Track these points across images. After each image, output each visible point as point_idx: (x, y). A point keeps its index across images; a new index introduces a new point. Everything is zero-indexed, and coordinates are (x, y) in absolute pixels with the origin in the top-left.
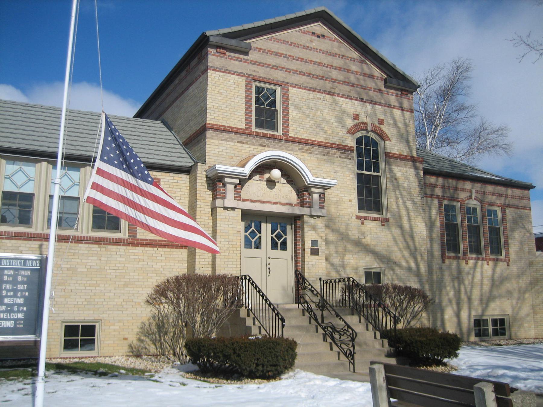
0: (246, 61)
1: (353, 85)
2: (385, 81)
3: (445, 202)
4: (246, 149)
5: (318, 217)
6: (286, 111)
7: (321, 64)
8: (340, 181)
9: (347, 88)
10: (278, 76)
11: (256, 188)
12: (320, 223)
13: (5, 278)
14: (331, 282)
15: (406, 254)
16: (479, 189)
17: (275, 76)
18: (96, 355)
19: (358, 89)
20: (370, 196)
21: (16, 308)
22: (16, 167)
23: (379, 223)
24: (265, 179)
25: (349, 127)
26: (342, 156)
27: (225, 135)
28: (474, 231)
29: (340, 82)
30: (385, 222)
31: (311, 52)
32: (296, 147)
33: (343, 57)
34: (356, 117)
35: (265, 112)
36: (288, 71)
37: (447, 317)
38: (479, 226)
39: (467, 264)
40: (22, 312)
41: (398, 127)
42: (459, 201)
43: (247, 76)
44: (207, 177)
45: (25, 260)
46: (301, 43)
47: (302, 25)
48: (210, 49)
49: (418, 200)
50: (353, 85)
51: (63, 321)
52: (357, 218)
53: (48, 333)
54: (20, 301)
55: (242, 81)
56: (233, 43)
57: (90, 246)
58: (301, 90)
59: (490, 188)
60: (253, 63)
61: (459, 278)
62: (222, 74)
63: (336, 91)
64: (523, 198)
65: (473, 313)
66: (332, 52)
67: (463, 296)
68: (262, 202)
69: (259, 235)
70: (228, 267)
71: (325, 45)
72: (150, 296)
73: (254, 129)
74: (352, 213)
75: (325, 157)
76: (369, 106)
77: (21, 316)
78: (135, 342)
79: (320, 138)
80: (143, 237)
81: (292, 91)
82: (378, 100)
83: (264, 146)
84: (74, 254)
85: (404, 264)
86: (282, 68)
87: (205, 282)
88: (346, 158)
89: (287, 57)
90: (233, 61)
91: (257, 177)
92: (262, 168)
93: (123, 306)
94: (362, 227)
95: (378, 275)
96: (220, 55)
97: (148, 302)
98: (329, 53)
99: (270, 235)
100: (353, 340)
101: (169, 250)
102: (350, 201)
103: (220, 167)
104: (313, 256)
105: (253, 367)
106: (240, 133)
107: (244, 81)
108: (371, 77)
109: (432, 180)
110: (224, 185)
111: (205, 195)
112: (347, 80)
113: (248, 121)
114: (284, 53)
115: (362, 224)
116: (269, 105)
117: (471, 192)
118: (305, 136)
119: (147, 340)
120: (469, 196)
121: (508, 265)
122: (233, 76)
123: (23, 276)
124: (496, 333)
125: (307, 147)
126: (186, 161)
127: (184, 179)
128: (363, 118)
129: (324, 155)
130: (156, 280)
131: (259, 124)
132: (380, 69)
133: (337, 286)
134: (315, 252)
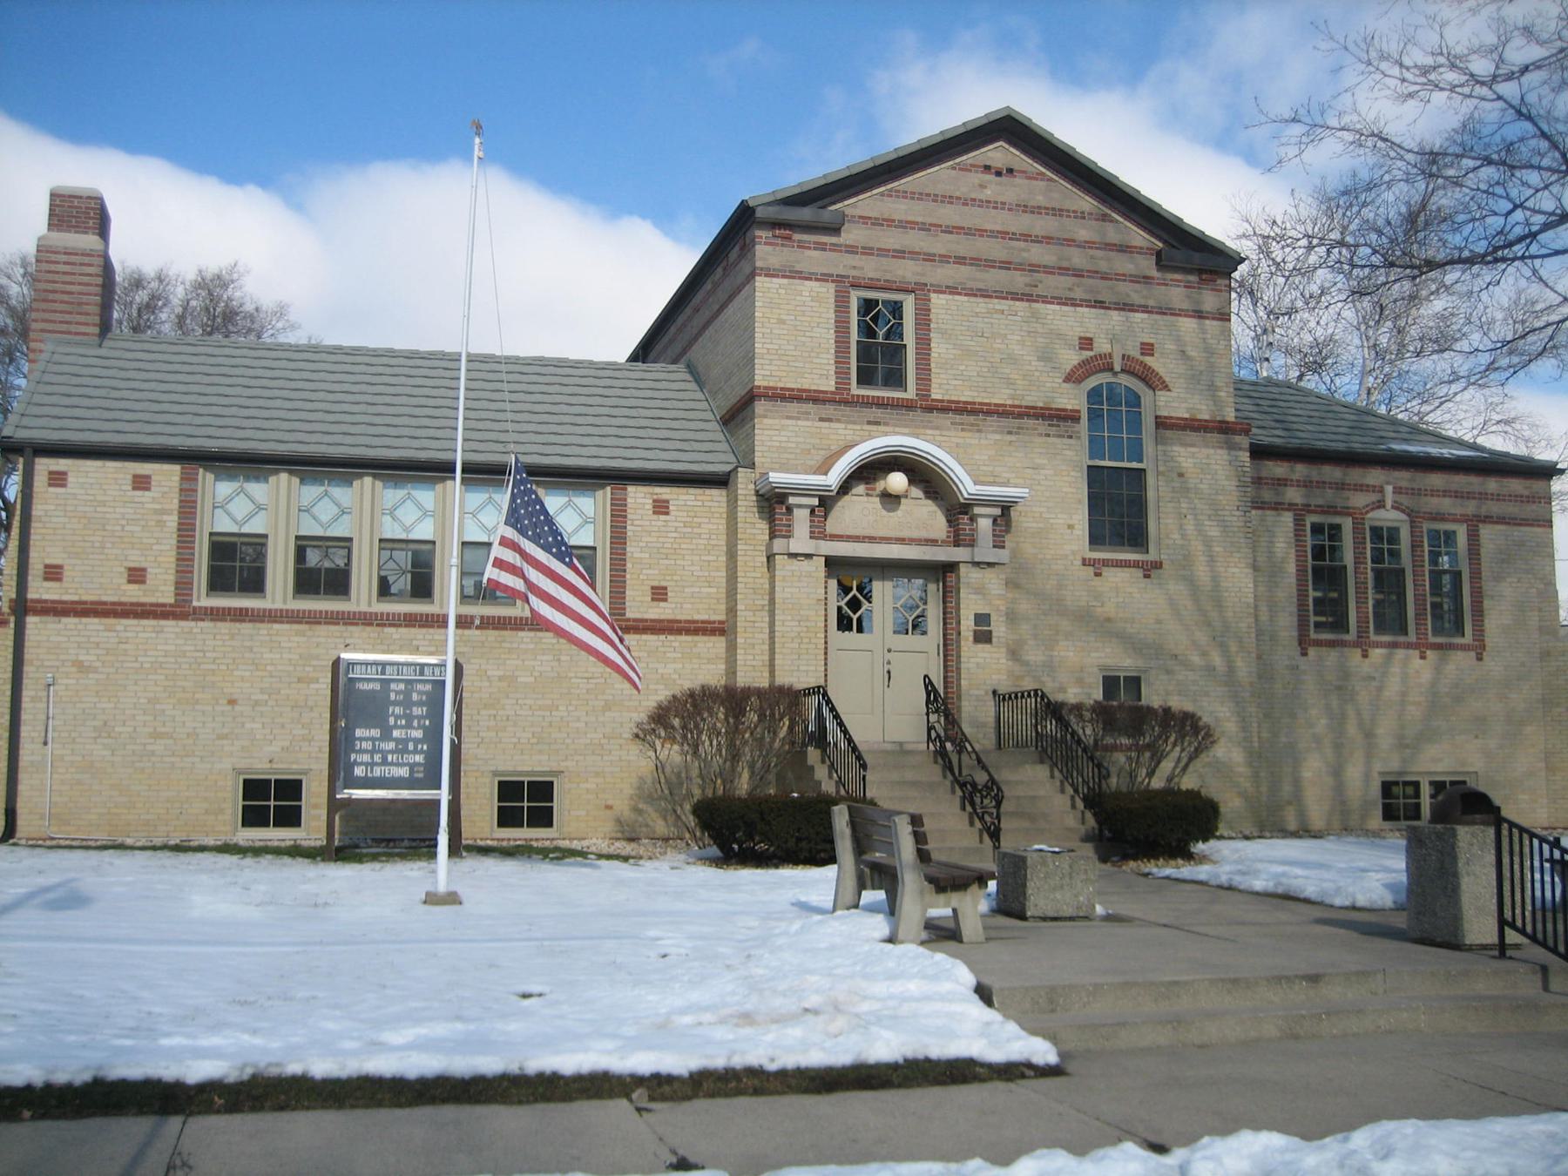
0: (835, 248)
1: (1078, 274)
2: (1159, 254)
3: (1311, 519)
4: (839, 431)
5: (990, 565)
6: (924, 344)
7: (1003, 234)
8: (1046, 489)
9: (1067, 281)
10: (907, 271)
11: (858, 512)
12: (993, 581)
13: (393, 696)
15: (1202, 637)
16: (1404, 484)
17: (900, 272)
18: (556, 835)
19: (1091, 281)
20: (1118, 512)
21: (411, 746)
22: (401, 493)
23: (1139, 573)
24: (878, 491)
25: (1068, 368)
26: (1053, 430)
27: (794, 407)
28: (1389, 581)
29: (1049, 270)
30: (1150, 569)
32: (945, 420)
33: (1057, 212)
34: (1086, 343)
35: (879, 351)
36: (929, 258)
37: (1307, 774)
38: (1403, 570)
39: (1365, 656)
40: (422, 752)
41: (1189, 358)
42: (1349, 514)
43: (839, 280)
44: (757, 493)
45: (422, 666)
46: (958, 194)
47: (960, 154)
48: (758, 233)
49: (1235, 519)
50: (1078, 274)
51: (495, 773)
52: (1085, 562)
54: (418, 734)
55: (828, 291)
56: (805, 214)
57: (540, 634)
58: (957, 297)
59: (1436, 480)
60: (851, 250)
61: (1342, 688)
62: (785, 281)
63: (1040, 291)
64: (1532, 499)
65: (1378, 767)
66: (1031, 203)
67: (1352, 729)
68: (872, 539)
69: (842, 604)
70: (798, 673)
71: (1011, 190)
72: (638, 725)
73: (856, 390)
74: (1074, 553)
75: (1013, 438)
76: (1116, 316)
77: (419, 758)
78: (627, 814)
79: (1001, 397)
80: (638, 616)
81: (937, 301)
82: (1143, 302)
83: (877, 423)
84: (510, 651)
85: (1196, 659)
86: (913, 255)
87: (734, 699)
88: (1060, 436)
89: (925, 228)
90: (808, 253)
91: (860, 489)
92: (870, 471)
93: (602, 745)
94: (1097, 581)
95: (1134, 683)
96: (779, 241)
97: (637, 736)
98: (1025, 208)
100: (998, 806)
101: (689, 638)
102: (1070, 527)
103: (776, 477)
104: (980, 646)
105: (791, 843)
106: (824, 401)
107: (832, 291)
108: (1124, 249)
109: (1278, 469)
110: (789, 510)
111: (754, 528)
112: (1065, 264)
113: (841, 374)
114: (920, 219)
115: (1098, 575)
116: (887, 336)
117: (1381, 491)
118: (966, 395)
119: (650, 810)
120: (1384, 503)
121: (1480, 659)
122: (807, 283)
123: (420, 693)
125: (972, 418)
126: (718, 464)
127: (716, 496)
128: (1102, 346)
129: (1010, 433)
130: (658, 694)
131: (865, 378)
132: (1145, 229)
134: (983, 637)
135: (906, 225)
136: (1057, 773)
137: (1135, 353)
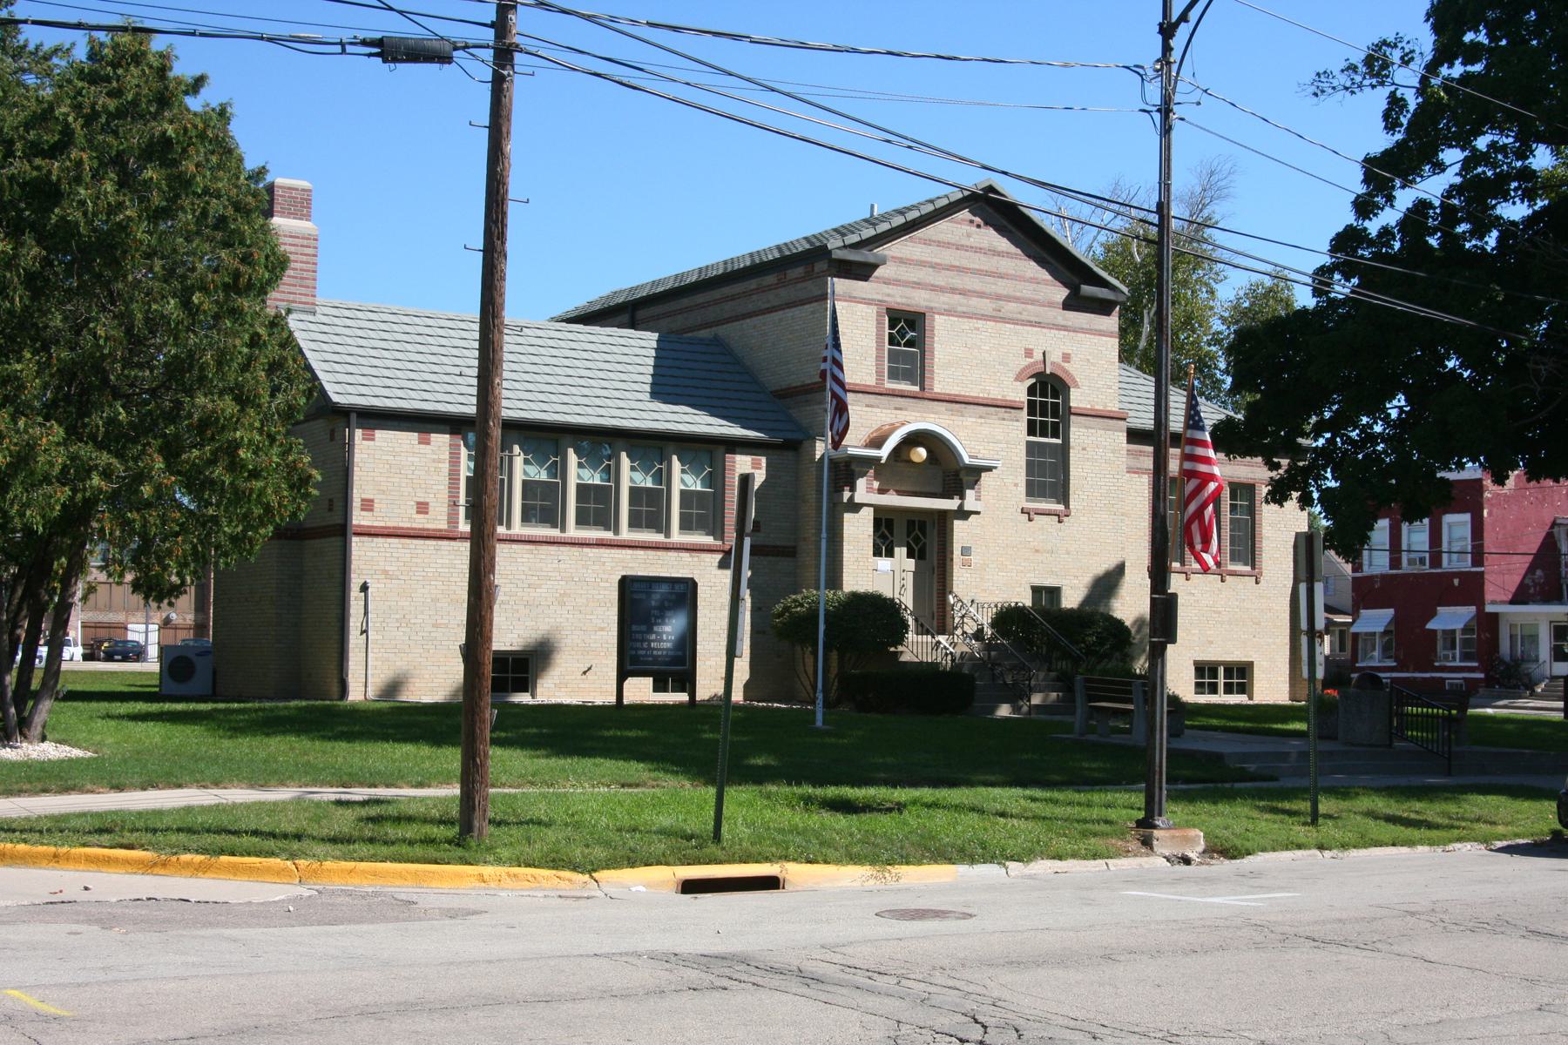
8: (996, 444)
20: (1049, 478)
36: (934, 288)
53: (107, 673)
89: (935, 266)
113: (879, 373)
124: (1213, 671)
131: (894, 375)
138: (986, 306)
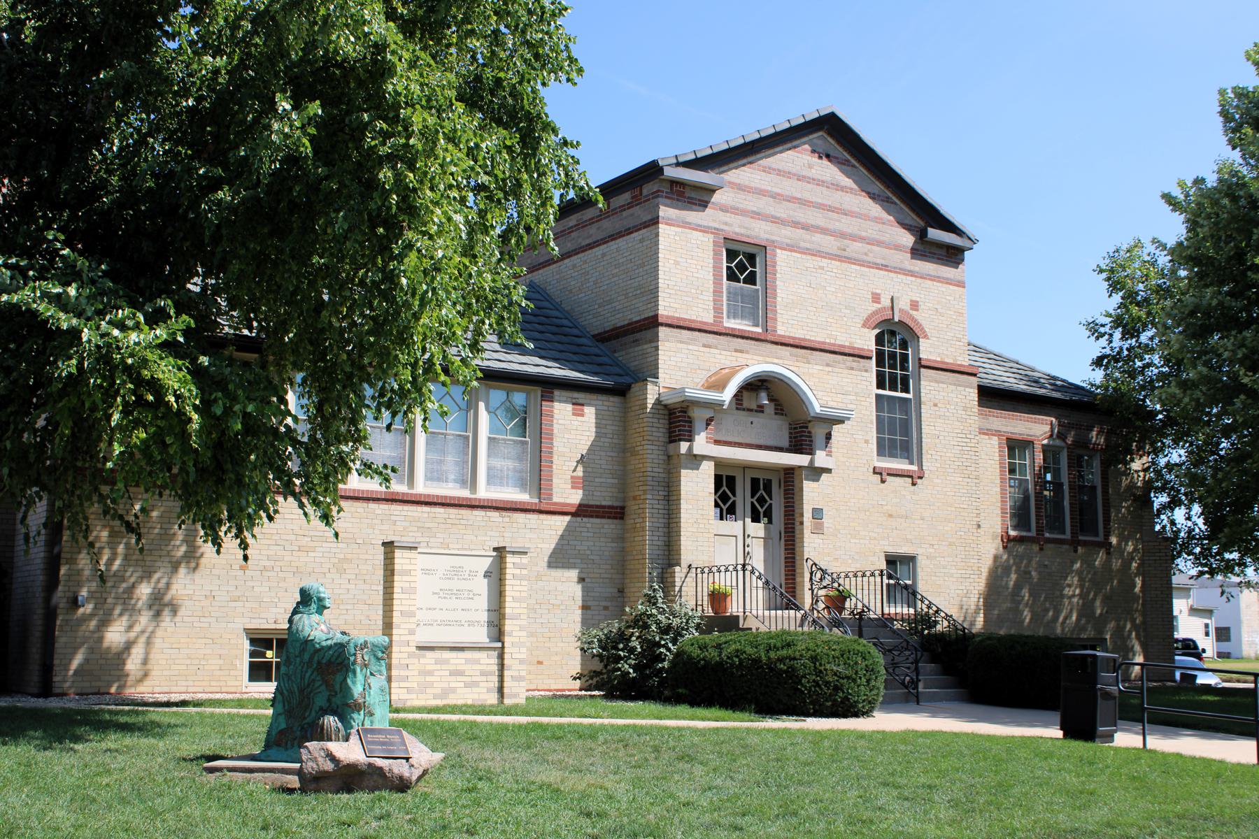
14: (710, 571)
31: (809, 186)
36: (775, 220)
62: (679, 230)
69: (733, 498)
83: (741, 351)
89: (775, 196)
99: (749, 500)
102: (867, 442)
113: (717, 310)
115: (883, 481)
129: (828, 365)
133: (859, 583)
135: (763, 193)
136: (310, 509)
137: (907, 307)
138: (829, 243)
